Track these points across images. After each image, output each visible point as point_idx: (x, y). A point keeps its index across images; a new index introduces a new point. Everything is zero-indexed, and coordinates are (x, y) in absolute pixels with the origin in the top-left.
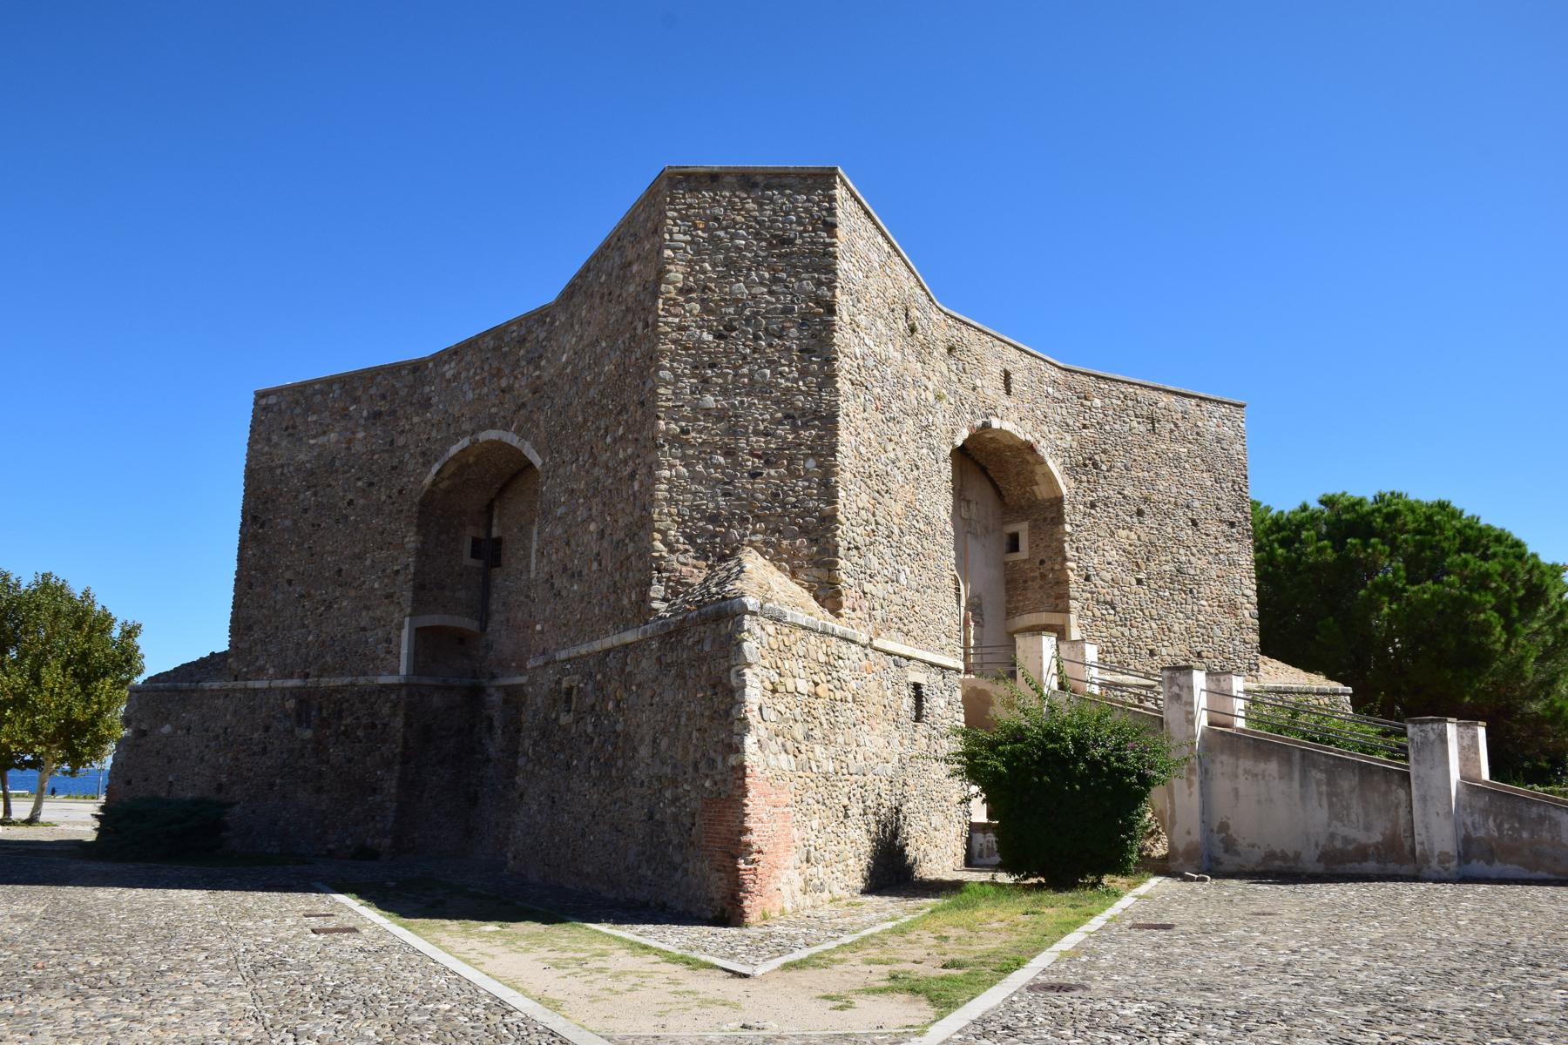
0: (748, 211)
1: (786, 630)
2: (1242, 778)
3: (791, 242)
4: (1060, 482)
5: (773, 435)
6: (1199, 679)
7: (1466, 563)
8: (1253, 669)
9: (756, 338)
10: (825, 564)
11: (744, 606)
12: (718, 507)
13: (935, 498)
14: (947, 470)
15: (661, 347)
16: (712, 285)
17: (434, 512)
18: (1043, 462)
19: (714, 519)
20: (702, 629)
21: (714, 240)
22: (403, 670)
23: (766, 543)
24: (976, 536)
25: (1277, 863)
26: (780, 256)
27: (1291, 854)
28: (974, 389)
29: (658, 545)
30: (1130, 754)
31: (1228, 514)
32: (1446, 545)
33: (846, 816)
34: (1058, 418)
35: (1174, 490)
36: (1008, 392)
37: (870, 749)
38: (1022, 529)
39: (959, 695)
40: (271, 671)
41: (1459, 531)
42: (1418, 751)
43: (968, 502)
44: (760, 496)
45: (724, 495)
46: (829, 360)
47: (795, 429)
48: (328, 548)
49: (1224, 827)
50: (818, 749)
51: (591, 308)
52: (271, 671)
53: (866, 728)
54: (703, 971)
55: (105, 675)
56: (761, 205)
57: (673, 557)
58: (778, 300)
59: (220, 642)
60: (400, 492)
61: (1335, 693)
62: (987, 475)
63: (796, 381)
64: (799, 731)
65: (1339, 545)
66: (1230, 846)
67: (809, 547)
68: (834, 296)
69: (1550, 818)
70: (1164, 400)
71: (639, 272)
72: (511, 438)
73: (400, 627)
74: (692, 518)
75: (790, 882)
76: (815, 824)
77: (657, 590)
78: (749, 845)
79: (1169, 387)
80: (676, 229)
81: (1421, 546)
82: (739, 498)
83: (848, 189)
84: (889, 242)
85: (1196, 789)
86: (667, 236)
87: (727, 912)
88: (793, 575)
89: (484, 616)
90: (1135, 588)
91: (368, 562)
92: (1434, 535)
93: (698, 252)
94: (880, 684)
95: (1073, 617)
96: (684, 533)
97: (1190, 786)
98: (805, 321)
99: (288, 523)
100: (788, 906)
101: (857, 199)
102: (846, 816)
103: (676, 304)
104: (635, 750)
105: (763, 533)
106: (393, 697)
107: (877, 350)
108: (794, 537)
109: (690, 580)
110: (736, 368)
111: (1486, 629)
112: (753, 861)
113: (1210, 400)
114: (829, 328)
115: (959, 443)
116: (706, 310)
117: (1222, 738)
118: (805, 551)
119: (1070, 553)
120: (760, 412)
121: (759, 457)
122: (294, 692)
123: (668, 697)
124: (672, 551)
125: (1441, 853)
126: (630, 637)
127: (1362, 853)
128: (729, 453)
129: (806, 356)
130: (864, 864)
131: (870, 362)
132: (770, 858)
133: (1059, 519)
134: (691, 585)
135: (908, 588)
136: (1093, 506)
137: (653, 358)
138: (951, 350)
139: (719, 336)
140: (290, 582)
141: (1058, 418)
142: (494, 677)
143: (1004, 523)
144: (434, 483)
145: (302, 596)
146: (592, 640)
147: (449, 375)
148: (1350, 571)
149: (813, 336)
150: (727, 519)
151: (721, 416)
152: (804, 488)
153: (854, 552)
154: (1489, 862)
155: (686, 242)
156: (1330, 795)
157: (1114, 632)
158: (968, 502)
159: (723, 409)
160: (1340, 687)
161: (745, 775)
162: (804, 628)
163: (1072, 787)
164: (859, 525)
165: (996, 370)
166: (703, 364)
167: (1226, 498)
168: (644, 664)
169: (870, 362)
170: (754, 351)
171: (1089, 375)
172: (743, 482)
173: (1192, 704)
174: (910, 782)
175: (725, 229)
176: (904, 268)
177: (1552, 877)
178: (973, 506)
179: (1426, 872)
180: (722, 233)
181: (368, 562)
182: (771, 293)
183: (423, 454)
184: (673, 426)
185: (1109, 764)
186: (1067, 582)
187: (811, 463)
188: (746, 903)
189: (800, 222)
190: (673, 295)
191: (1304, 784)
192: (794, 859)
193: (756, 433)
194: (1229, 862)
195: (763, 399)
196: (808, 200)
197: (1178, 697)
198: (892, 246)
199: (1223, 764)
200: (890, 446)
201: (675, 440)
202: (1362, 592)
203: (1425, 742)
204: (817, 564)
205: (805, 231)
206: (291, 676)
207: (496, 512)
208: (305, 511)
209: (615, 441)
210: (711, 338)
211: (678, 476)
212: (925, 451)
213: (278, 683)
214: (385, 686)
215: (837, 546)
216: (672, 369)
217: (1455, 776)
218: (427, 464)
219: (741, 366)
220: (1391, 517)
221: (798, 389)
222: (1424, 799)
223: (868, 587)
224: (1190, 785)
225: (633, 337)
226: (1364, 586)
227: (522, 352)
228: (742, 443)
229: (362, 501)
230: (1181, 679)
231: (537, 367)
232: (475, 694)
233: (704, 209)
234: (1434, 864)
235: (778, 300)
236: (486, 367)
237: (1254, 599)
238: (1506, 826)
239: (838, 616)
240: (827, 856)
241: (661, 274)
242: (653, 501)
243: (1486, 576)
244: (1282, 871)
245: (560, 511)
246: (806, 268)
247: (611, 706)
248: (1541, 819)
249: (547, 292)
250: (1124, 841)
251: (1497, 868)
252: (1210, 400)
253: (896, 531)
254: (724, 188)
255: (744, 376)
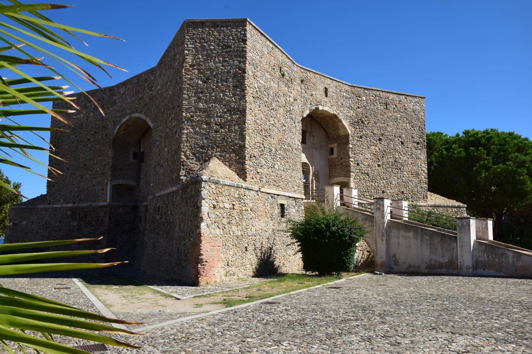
0: (215, 36)
1: (221, 187)
2: (401, 238)
3: (230, 47)
4: (348, 129)
5: (223, 117)
6: (387, 202)
7: (517, 157)
8: (425, 198)
9: (218, 82)
10: (241, 163)
11: (202, 179)
12: (204, 143)
13: (293, 137)
14: (299, 126)
15: (184, 86)
16: (202, 64)
17: (119, 143)
18: (341, 122)
19: (202, 147)
20: (192, 186)
21: (202, 47)
22: (108, 200)
23: (221, 156)
24: (316, 149)
25: (412, 269)
26: (226, 52)
27: (417, 266)
28: (312, 95)
29: (183, 157)
30: (346, 230)
31: (417, 139)
32: (509, 150)
33: (246, 250)
34: (348, 105)
35: (394, 131)
36: (326, 96)
37: (258, 227)
38: (335, 146)
39: (303, 208)
40: (62, 201)
41: (517, 144)
42: (460, 229)
43: (314, 136)
44: (218, 139)
45: (206, 139)
46: (243, 90)
47: (231, 115)
48: (81, 156)
49: (394, 256)
50: (233, 227)
51: (166, 70)
52: (62, 201)
53: (257, 220)
54: (10, 262)
55: (7, 202)
56: (219, 33)
57: (188, 161)
58: (225, 68)
59: (44, 191)
60: (106, 136)
61: (459, 207)
62: (322, 126)
63: (231, 98)
64: (225, 221)
65: (466, 149)
66: (396, 263)
67: (235, 157)
68: (245, 66)
69: (506, 254)
70: (391, 96)
71: (178, 58)
72: (143, 116)
73: (107, 185)
74: (195, 147)
75: (219, 272)
76: (231, 253)
77: (182, 173)
78: (202, 259)
79: (393, 92)
80: (189, 43)
81: (500, 150)
82: (211, 140)
83: (253, 26)
84: (272, 43)
85: (384, 242)
86: (186, 46)
87: (193, 281)
88: (230, 167)
89: (138, 180)
90: (377, 168)
91: (95, 161)
92: (505, 146)
93: (197, 51)
94: (264, 205)
95: (352, 179)
96: (192, 153)
97: (382, 241)
98: (235, 76)
99: (66, 147)
100: (218, 280)
101: (256, 29)
102: (246, 250)
103: (189, 71)
104: (175, 228)
105: (220, 152)
106: (105, 210)
107: (266, 84)
108: (231, 153)
109: (194, 169)
110: (210, 93)
111: (524, 182)
112: (203, 265)
113: (411, 96)
114: (243, 78)
115: (305, 115)
116: (200, 72)
117: (396, 224)
118: (234, 158)
119: (351, 155)
120: (219, 109)
121: (218, 125)
122: (70, 209)
123: (183, 209)
124: (188, 159)
125: (467, 266)
126: (174, 189)
127: (441, 266)
128: (208, 124)
129: (235, 88)
130: (254, 267)
131: (262, 89)
132: (211, 264)
133: (348, 143)
134: (194, 171)
135: (279, 169)
136: (361, 137)
137: (181, 90)
138: (302, 81)
139: (204, 82)
140: (68, 169)
141: (348, 105)
142: (142, 202)
143: (329, 144)
144: (118, 132)
145: (72, 174)
146: (165, 189)
147: (122, 92)
148: (472, 160)
149: (238, 81)
150: (207, 147)
151: (205, 111)
152: (234, 136)
153: (254, 158)
154: (484, 269)
155: (192, 48)
156: (430, 245)
157: (368, 184)
158: (314, 136)
159: (206, 108)
160: (461, 205)
161: (201, 236)
162: (229, 186)
163: (325, 241)
164: (255, 148)
165: (322, 88)
166: (198, 92)
167: (416, 133)
168: (178, 198)
169: (262, 89)
170: (217, 87)
171: (361, 88)
172: (213, 134)
173: (384, 211)
174: (277, 239)
175: (206, 42)
176: (280, 52)
177: (505, 275)
178: (316, 139)
179: (396, 268)
180: (205, 44)
181: (95, 161)
182: (223, 66)
183: (114, 122)
184: (188, 114)
185: (338, 233)
186: (350, 166)
187: (237, 127)
188: (200, 278)
189: (233, 39)
190: (188, 67)
191: (422, 241)
192: (221, 264)
193: (217, 117)
194: (396, 268)
195: (220, 104)
196: (236, 31)
197: (379, 209)
198: (274, 45)
199: (394, 233)
200: (271, 119)
201: (189, 119)
202: (475, 168)
203: (463, 226)
204: (238, 163)
205: (235, 43)
206: (69, 203)
207: (142, 142)
208: (73, 143)
209: (172, 119)
210: (201, 83)
211: (190, 132)
212: (288, 120)
213: (64, 205)
214: (102, 206)
215: (245, 156)
216: (188, 94)
217: (473, 237)
218: (115, 126)
219: (212, 93)
220: (489, 139)
221: (232, 100)
222: (461, 247)
223: (259, 170)
224: (382, 241)
225: (177, 82)
226: (475, 166)
227: (146, 85)
228: (212, 120)
229: (93, 139)
230: (380, 202)
231: (151, 90)
232: (136, 208)
233: (199, 35)
234: (464, 270)
235: (225, 68)
236: (134, 90)
237: (426, 171)
238: (490, 257)
239: (246, 181)
240: (237, 264)
241: (184, 59)
242: (181, 142)
243: (524, 162)
244: (412, 271)
245: (158, 143)
246: (235, 56)
247: (169, 213)
248: (503, 254)
249: (154, 64)
250: (345, 260)
251: (487, 272)
252: (411, 96)
253: (274, 149)
254: (206, 27)
255: (213, 96)
